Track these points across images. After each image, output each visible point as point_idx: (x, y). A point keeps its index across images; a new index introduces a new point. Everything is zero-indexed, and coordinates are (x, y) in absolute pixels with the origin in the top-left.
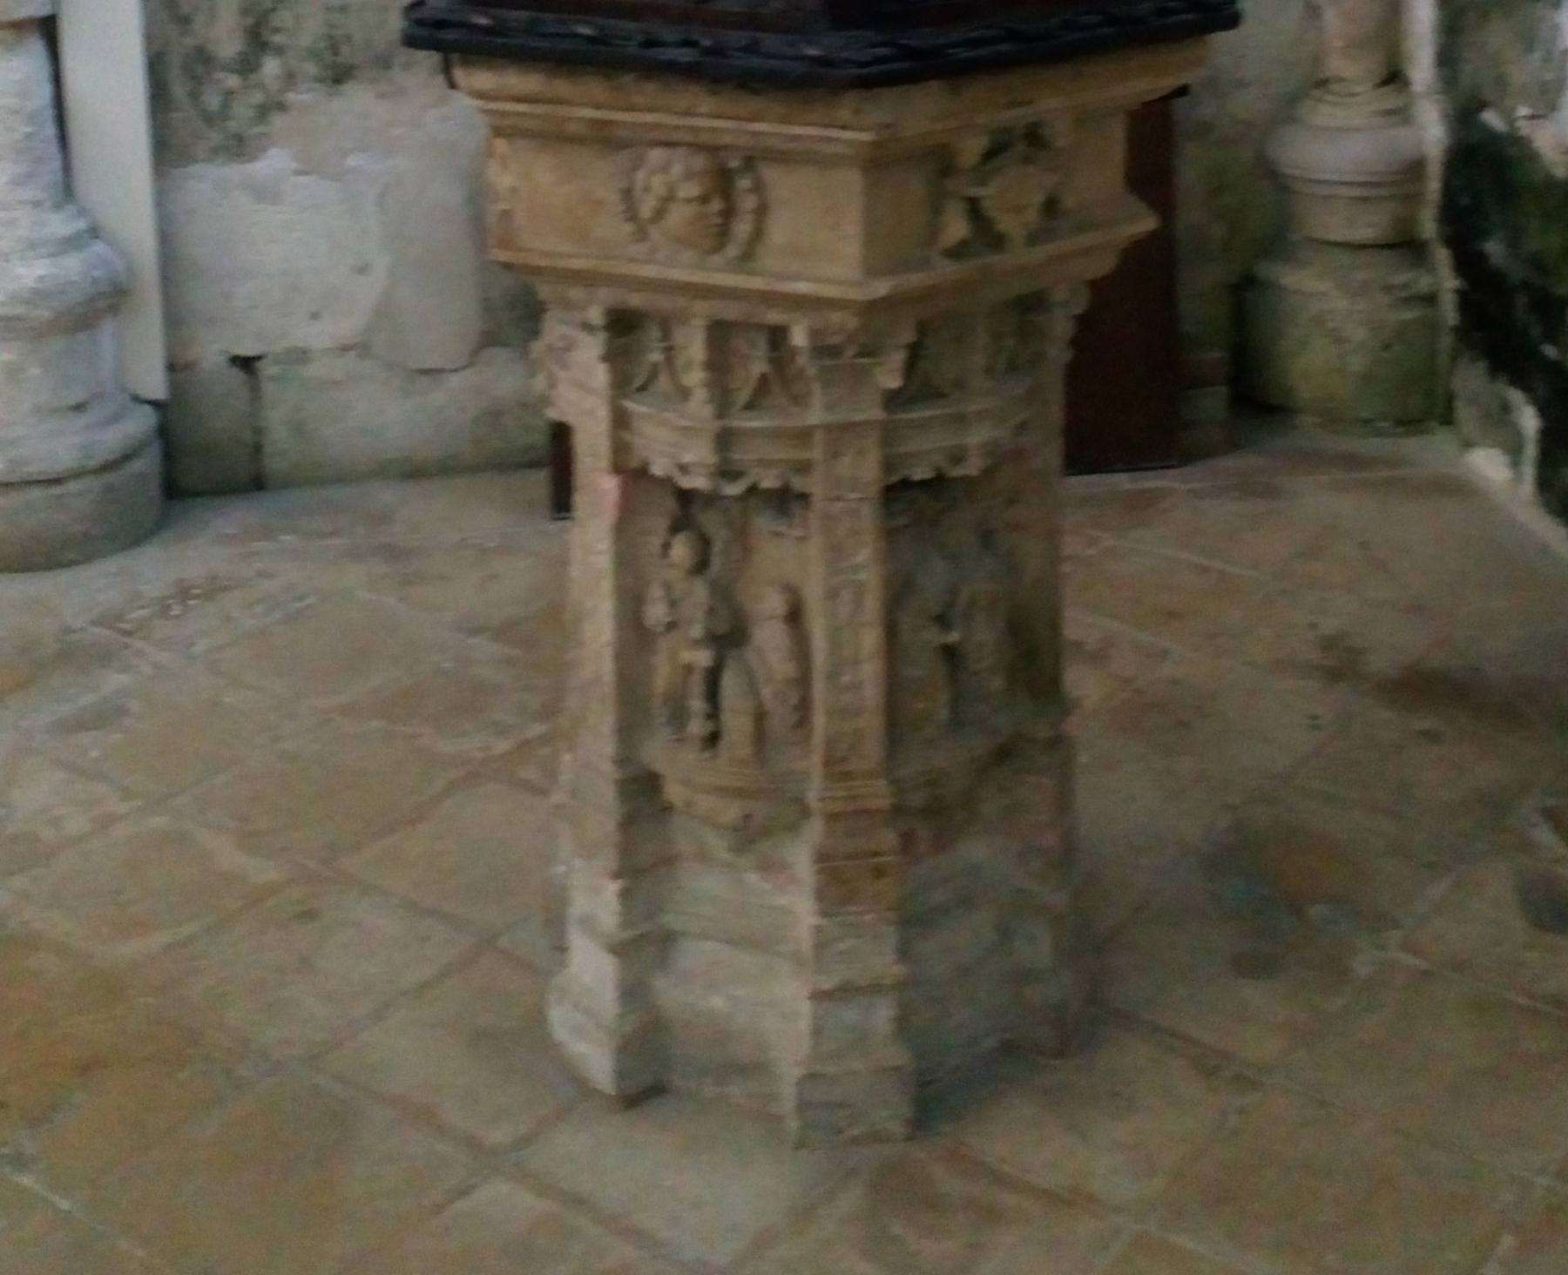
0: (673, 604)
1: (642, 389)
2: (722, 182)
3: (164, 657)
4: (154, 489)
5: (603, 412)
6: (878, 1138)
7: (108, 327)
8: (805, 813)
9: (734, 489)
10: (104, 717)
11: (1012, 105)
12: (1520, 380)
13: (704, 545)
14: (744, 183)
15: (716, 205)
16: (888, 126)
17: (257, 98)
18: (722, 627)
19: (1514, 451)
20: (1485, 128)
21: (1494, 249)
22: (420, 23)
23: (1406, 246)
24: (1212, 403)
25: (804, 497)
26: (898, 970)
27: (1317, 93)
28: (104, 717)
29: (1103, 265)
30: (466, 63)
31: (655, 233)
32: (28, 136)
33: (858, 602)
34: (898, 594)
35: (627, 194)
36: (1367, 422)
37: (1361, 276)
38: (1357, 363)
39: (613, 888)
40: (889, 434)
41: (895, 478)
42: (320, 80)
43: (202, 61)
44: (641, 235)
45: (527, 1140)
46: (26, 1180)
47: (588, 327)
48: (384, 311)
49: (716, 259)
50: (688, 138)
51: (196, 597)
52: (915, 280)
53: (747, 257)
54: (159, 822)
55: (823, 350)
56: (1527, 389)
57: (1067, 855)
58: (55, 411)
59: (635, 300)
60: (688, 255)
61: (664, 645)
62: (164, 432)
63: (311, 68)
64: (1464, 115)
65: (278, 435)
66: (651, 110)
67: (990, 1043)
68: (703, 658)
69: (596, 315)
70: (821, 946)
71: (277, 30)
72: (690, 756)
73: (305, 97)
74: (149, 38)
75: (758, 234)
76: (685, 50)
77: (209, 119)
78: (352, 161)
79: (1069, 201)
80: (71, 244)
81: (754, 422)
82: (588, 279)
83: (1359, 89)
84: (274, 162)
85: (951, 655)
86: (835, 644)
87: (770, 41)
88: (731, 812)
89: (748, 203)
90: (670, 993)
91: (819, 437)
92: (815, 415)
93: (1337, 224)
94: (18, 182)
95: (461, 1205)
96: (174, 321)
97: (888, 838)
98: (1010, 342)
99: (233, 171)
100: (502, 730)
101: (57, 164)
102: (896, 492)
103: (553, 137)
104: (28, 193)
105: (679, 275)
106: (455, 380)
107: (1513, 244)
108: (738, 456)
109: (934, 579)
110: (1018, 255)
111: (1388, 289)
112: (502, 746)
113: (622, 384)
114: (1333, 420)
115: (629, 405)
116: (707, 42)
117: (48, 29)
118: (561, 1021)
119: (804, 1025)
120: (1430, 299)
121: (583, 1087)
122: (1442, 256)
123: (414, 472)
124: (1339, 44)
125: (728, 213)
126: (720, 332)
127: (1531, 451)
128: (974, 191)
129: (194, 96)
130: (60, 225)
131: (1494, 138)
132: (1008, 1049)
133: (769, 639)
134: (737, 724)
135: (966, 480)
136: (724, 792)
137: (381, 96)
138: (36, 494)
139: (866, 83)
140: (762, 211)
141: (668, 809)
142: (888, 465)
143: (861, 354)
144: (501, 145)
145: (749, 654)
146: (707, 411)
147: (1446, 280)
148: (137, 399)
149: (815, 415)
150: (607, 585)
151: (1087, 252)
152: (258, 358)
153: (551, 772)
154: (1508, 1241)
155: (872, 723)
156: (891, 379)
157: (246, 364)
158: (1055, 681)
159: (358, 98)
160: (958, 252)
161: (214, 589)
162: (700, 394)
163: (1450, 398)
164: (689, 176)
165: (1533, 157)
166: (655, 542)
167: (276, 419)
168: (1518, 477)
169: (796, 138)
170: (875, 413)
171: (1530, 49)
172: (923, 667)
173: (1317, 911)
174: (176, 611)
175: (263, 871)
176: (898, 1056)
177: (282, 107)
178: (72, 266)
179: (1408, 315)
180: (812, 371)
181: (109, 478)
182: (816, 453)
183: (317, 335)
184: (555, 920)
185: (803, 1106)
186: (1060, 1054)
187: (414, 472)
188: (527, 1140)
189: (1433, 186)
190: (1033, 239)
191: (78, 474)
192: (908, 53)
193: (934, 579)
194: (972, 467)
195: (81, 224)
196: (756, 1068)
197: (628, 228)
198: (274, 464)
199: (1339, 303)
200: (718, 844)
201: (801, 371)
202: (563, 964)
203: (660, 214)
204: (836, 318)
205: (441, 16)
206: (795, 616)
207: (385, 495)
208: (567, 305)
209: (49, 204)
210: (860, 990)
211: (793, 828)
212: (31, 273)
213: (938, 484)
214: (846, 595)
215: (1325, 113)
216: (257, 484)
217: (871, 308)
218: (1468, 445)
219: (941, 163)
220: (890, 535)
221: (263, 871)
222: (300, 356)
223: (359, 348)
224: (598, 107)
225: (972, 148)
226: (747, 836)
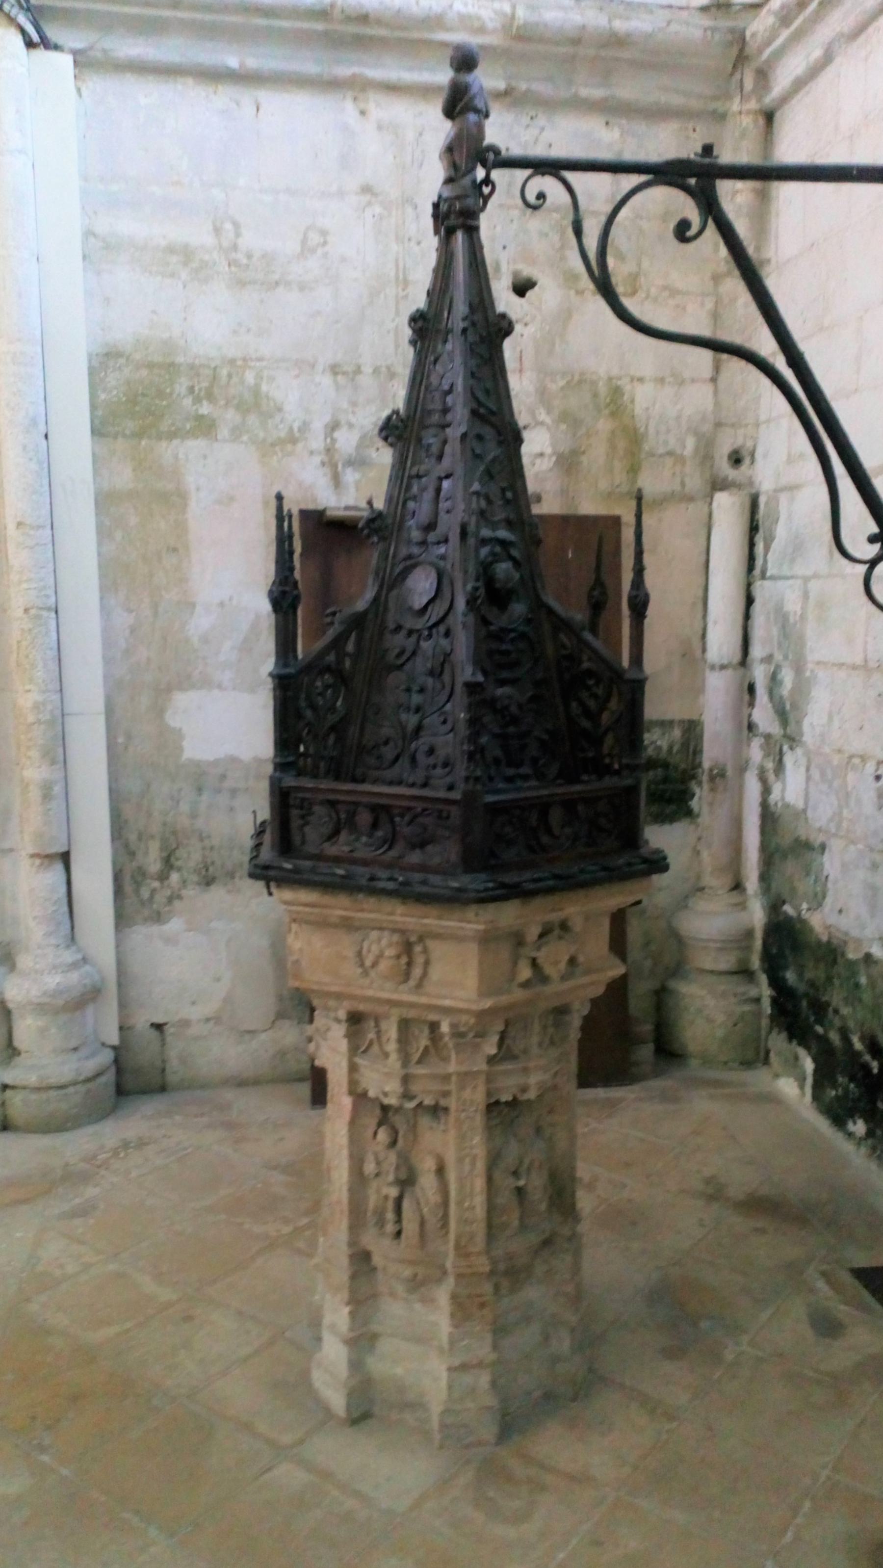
0: (378, 1163)
1: (364, 1052)
2: (408, 948)
3: (115, 1180)
4: (112, 1089)
5: (344, 1064)
6: (480, 1443)
7: (90, 1010)
8: (445, 1273)
9: (411, 1105)
10: (83, 1212)
11: (553, 910)
12: (803, 1042)
13: (395, 1132)
14: (418, 949)
15: (404, 960)
16: (492, 922)
17: (168, 893)
18: (403, 1176)
19: (801, 1081)
20: (785, 913)
21: (790, 976)
22: (256, 866)
23: (744, 972)
24: (646, 1052)
25: (446, 1110)
26: (493, 1357)
27: (699, 894)
28: (83, 1212)
29: (600, 990)
30: (279, 886)
31: (373, 974)
32: (55, 911)
33: (473, 1164)
34: (494, 1160)
35: (359, 954)
36: (726, 1063)
37: (723, 987)
38: (720, 1033)
39: (346, 1310)
40: (489, 1080)
41: (492, 1100)
42: (199, 884)
43: (141, 874)
44: (366, 973)
45: (301, 1442)
46: (45, 1458)
47: (338, 1021)
48: (228, 1000)
49: (404, 987)
50: (391, 926)
51: (132, 1147)
52: (504, 999)
53: (419, 985)
54: (112, 1267)
55: (457, 1034)
56: (808, 1048)
57: (577, 1299)
58: (65, 1051)
59: (362, 1007)
60: (389, 985)
61: (374, 1185)
62: (116, 1061)
63: (195, 878)
64: (774, 907)
65: (174, 1064)
66: (371, 911)
67: (537, 1394)
68: (394, 1192)
69: (342, 1014)
70: (452, 1342)
71: (177, 859)
72: (387, 1242)
73: (192, 893)
74: (114, 863)
75: (425, 974)
76: (389, 883)
77: (143, 903)
78: (214, 924)
79: (581, 959)
80: (74, 966)
81: (421, 1071)
82: (339, 996)
83: (720, 892)
84: (175, 925)
85: (520, 1192)
86: (461, 1188)
87: (435, 879)
88: (407, 1272)
89: (419, 960)
90: (376, 1366)
91: (454, 1079)
92: (452, 1067)
93: (707, 961)
94: (48, 934)
95: (267, 1476)
96: (123, 1005)
97: (487, 1288)
98: (551, 1030)
99: (155, 929)
100: (286, 1221)
101: (68, 926)
102: (493, 1107)
103: (322, 924)
104: (53, 941)
105: (385, 995)
106: (263, 1036)
107: (800, 975)
108: (415, 1088)
109: (513, 1151)
110: (555, 987)
111: (735, 995)
112: (287, 1229)
113: (354, 1050)
114: (707, 1061)
115: (359, 1060)
116: (401, 879)
117: (65, 858)
118: (318, 1378)
119: (444, 1383)
120: (757, 1000)
121: (328, 1411)
122: (763, 979)
123: (241, 1083)
124: (710, 869)
125: (409, 964)
126: (405, 1025)
127: (809, 1081)
128: (534, 954)
129: (137, 891)
130: (69, 956)
131: (789, 919)
132: (548, 1396)
133: (427, 1182)
134: (410, 1226)
135: (529, 1101)
136: (402, 1261)
137: (229, 892)
138: (53, 1093)
139: (482, 901)
140: (427, 963)
141: (374, 1269)
142: (489, 1094)
143: (476, 1036)
144: (294, 927)
145: (417, 1189)
146: (398, 1065)
147: (766, 992)
148: (103, 1044)
149: (452, 1067)
150: (345, 1152)
151: (592, 983)
152: (165, 1024)
153: (313, 1244)
154: (807, 1505)
155: (479, 1229)
156: (490, 1048)
157: (159, 1027)
158: (573, 1205)
159: (217, 894)
160: (526, 985)
161: (141, 1144)
162: (394, 1057)
163: (767, 1052)
164: (390, 945)
165: (811, 930)
166: (370, 1132)
167: (173, 1053)
168: (803, 1094)
169: (444, 927)
170: (484, 1067)
171: (808, 874)
172: (505, 1198)
173: (704, 1324)
174: (122, 1155)
175: (166, 1295)
176: (490, 1400)
177: (179, 897)
178: (74, 977)
179: (747, 1008)
180: (451, 1045)
181: (89, 1085)
182: (453, 1087)
183: (195, 1013)
184: (316, 1323)
185: (443, 1426)
186: (574, 1399)
187: (241, 1083)
188: (301, 1442)
189: (758, 943)
190: (563, 978)
191: (75, 1083)
192: (503, 886)
193: (513, 1151)
194: (532, 1095)
195: (79, 956)
196: (417, 1405)
197: (360, 970)
198: (172, 1078)
199: (710, 1002)
200: (400, 1289)
201: (446, 1045)
202: (320, 1348)
203: (374, 964)
204: (464, 1018)
205: (268, 863)
206: (440, 1171)
207: (229, 1095)
208: (327, 1009)
209: (62, 946)
210: (473, 1367)
211: (439, 1281)
212: (53, 981)
213: (514, 1103)
214: (467, 1160)
215: (701, 904)
216: (163, 1089)
217: (481, 1015)
218: (777, 1076)
219: (518, 940)
220: (489, 1129)
221: (166, 1295)
222: (185, 1023)
223: (215, 1019)
224: (346, 909)
225: (533, 932)
226: (416, 1284)
